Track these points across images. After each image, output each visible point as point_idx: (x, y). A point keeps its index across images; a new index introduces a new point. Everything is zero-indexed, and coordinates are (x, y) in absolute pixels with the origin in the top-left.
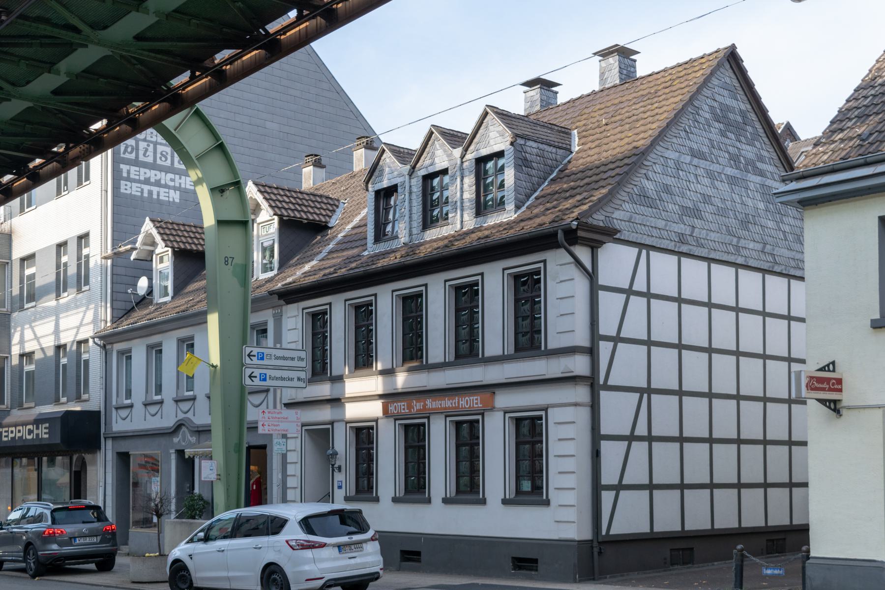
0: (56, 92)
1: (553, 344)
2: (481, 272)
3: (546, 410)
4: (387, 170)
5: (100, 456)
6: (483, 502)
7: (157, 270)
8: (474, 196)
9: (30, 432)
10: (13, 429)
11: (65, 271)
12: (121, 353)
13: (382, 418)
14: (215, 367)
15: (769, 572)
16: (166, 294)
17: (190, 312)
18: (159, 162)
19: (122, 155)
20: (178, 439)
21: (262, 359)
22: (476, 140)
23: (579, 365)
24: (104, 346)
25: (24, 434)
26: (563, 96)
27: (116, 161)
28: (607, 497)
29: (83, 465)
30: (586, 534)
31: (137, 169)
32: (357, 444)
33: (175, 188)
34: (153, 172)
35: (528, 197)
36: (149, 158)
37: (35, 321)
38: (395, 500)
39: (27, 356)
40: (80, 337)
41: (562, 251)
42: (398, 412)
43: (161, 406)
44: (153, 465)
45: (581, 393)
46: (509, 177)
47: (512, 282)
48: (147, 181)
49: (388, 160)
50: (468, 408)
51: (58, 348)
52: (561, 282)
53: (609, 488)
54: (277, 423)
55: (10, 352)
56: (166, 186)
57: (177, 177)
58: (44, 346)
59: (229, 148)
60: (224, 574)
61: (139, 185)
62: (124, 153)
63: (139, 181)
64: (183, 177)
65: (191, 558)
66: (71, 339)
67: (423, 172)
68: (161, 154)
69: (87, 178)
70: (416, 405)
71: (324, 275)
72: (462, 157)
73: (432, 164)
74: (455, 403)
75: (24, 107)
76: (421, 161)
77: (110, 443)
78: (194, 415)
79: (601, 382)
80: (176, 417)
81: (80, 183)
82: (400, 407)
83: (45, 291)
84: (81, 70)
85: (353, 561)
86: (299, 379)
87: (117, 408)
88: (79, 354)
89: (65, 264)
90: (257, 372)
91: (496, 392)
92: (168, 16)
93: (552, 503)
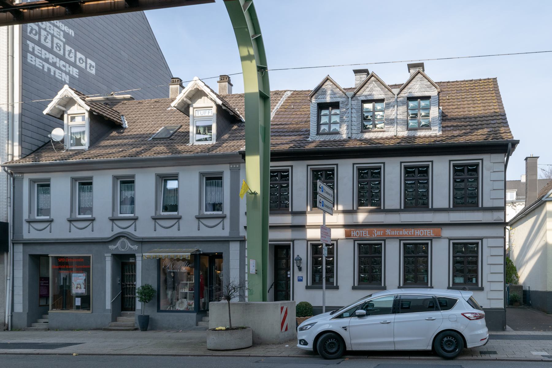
1: (486, 205)
2: (336, 163)
3: (481, 239)
4: (329, 92)
7: (68, 126)
12: (32, 181)
13: (342, 239)
14: (255, 193)
17: (141, 157)
18: (55, 49)
19: (28, 34)
20: (115, 247)
22: (408, 86)
24: (12, 174)
31: (40, 49)
36: (48, 44)
42: (360, 236)
43: (223, 220)
47: (313, 174)
48: (46, 60)
50: (359, 237)
52: (494, 172)
54: (325, 236)
56: (59, 69)
57: (67, 65)
60: (391, 339)
61: (41, 61)
63: (40, 58)
64: (71, 67)
65: (346, 329)
67: (363, 98)
68: (57, 45)
70: (377, 233)
74: (411, 233)
76: (361, 91)
77: (19, 249)
78: (135, 231)
80: (112, 231)
82: (364, 233)
91: (443, 228)
93: (485, 289)
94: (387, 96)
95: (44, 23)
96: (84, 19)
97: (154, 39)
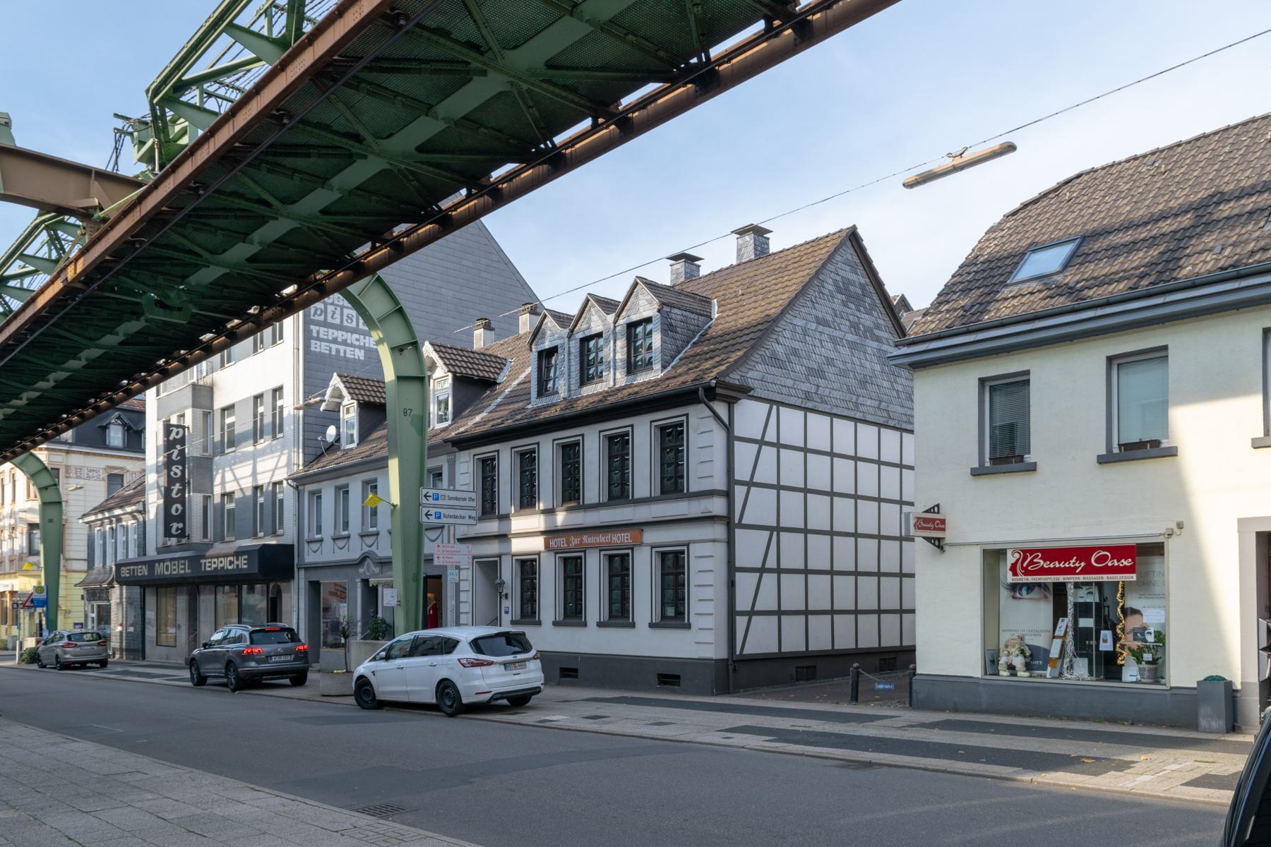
0: (250, 260)
1: (694, 487)
2: (537, 441)
3: (688, 545)
5: (294, 585)
6: (633, 625)
7: (344, 420)
8: (625, 356)
9: (231, 563)
10: (216, 560)
11: (262, 420)
12: (312, 493)
14: (395, 506)
15: (881, 687)
16: (353, 442)
17: (374, 457)
18: (345, 323)
19: (312, 317)
21: (437, 499)
22: (627, 307)
23: (717, 506)
24: (297, 487)
25: (225, 564)
26: (705, 269)
27: (307, 322)
28: (741, 622)
29: (279, 592)
30: (723, 654)
31: (326, 329)
32: (663, 568)
33: (360, 347)
34: (340, 333)
35: (673, 358)
37: (234, 464)
38: (556, 624)
39: (228, 495)
40: (275, 479)
41: (702, 406)
44: (341, 593)
45: (719, 531)
46: (656, 340)
48: (335, 341)
49: (549, 324)
51: (256, 488)
53: (742, 613)
55: (212, 492)
56: (352, 345)
57: (362, 337)
58: (243, 487)
59: (407, 311)
60: (404, 688)
61: (327, 344)
62: (314, 316)
63: (327, 341)
66: (267, 480)
67: (580, 335)
69: (281, 338)
71: (493, 426)
72: (615, 322)
73: (588, 328)
75: (221, 273)
77: (302, 573)
79: (736, 522)
81: (274, 342)
82: (560, 542)
83: (243, 438)
84: (463, 114)
85: (517, 677)
86: (470, 517)
87: (309, 542)
88: (274, 493)
89: (262, 414)
90: (432, 511)
92: (94, 360)
93: (693, 626)
94: (606, 327)
95: (331, 296)
96: (457, 233)
97: (500, 252)
